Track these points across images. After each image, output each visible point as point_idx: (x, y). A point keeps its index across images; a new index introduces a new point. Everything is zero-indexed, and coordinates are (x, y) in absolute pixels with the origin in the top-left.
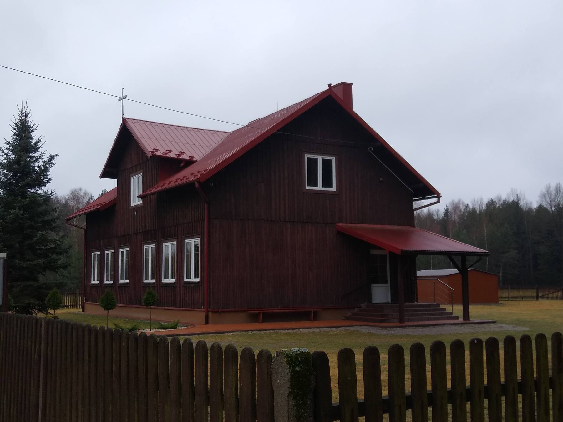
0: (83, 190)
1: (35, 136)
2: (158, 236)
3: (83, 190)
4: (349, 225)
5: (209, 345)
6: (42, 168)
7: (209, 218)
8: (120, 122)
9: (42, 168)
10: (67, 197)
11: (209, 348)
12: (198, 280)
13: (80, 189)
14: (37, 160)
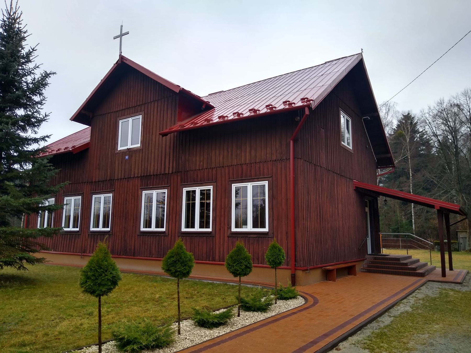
1: (27, 46)
2: (151, 181)
7: (294, 158)
9: (31, 85)
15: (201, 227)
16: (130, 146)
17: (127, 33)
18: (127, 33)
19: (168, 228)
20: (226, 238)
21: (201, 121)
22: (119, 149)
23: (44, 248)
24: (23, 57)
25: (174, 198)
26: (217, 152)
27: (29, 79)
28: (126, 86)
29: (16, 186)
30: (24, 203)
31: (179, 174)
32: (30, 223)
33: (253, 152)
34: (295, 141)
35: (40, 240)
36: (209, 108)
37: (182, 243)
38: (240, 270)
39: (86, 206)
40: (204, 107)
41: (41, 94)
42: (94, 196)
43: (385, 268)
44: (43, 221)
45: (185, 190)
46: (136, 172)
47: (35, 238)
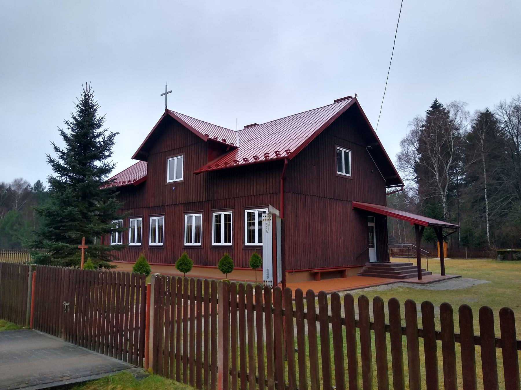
0: (24, 180)
1: (99, 115)
2: (191, 207)
3: (24, 180)
4: (379, 206)
5: (316, 292)
6: (102, 143)
7: (284, 192)
8: (164, 111)
9: (102, 143)
10: (12, 184)
11: (305, 295)
12: (140, 244)
13: (22, 179)
14: (98, 136)
15: (225, 242)
16: (175, 180)
17: (171, 92)
18: (171, 92)
19: (203, 243)
20: (241, 250)
21: (221, 163)
22: (168, 181)
23: (116, 258)
24: (96, 124)
25: (207, 220)
26: (235, 186)
27: (101, 139)
28: (169, 133)
29: (96, 215)
30: (102, 228)
31: (210, 202)
32: (105, 241)
33: (258, 186)
34: (284, 180)
35: (113, 252)
36: (233, 149)
37: (186, 254)
38: (225, 269)
39: (146, 224)
40: (228, 149)
41: (109, 150)
42: (151, 218)
43: (383, 273)
44: (114, 241)
45: (214, 214)
46: (180, 200)
47: (110, 251)
